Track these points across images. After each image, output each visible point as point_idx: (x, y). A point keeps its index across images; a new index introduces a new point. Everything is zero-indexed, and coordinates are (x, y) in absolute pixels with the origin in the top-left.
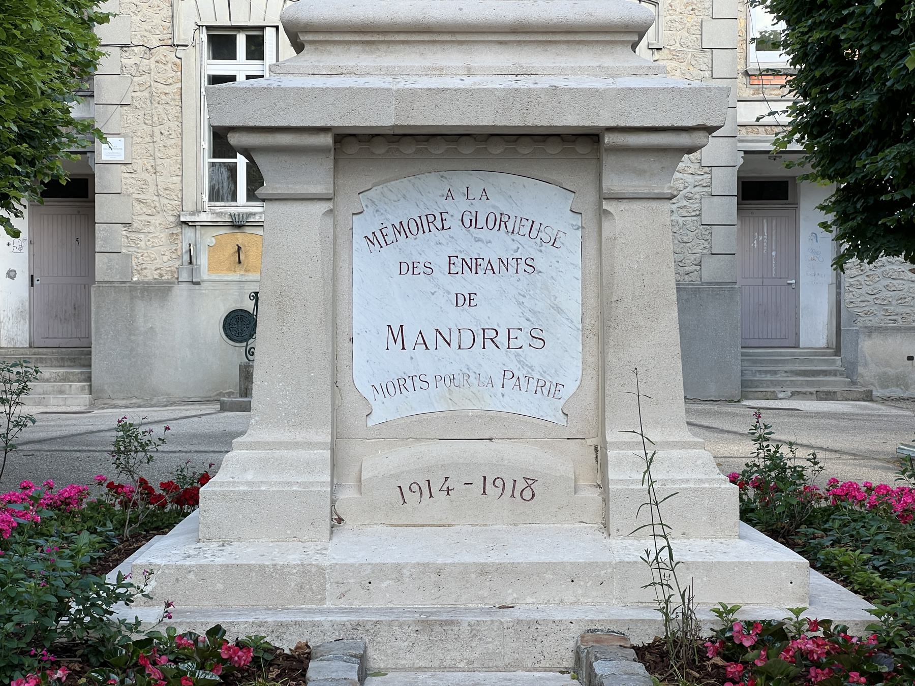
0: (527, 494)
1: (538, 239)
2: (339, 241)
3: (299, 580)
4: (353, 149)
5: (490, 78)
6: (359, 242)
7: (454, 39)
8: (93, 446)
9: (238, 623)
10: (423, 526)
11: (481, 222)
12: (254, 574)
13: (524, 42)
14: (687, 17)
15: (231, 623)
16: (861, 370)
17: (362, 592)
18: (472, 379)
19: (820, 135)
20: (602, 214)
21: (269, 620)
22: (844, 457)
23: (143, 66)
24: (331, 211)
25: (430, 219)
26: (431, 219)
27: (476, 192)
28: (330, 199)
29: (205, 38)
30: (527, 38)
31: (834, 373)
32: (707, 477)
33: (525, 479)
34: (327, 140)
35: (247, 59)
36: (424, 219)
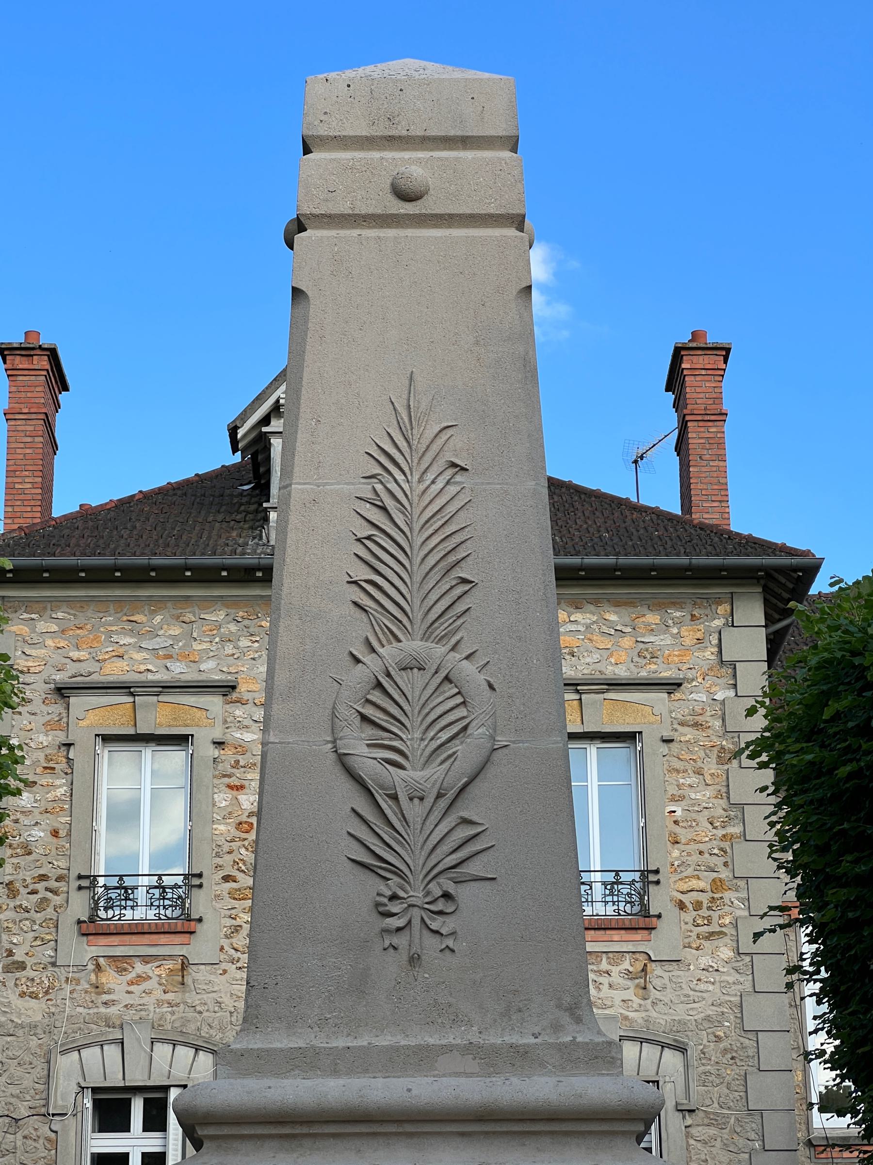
7: (401, 1130)
13: (494, 1133)
14: (726, 1069)
23: (6, 1144)
29: (89, 1104)
35: (144, 1131)
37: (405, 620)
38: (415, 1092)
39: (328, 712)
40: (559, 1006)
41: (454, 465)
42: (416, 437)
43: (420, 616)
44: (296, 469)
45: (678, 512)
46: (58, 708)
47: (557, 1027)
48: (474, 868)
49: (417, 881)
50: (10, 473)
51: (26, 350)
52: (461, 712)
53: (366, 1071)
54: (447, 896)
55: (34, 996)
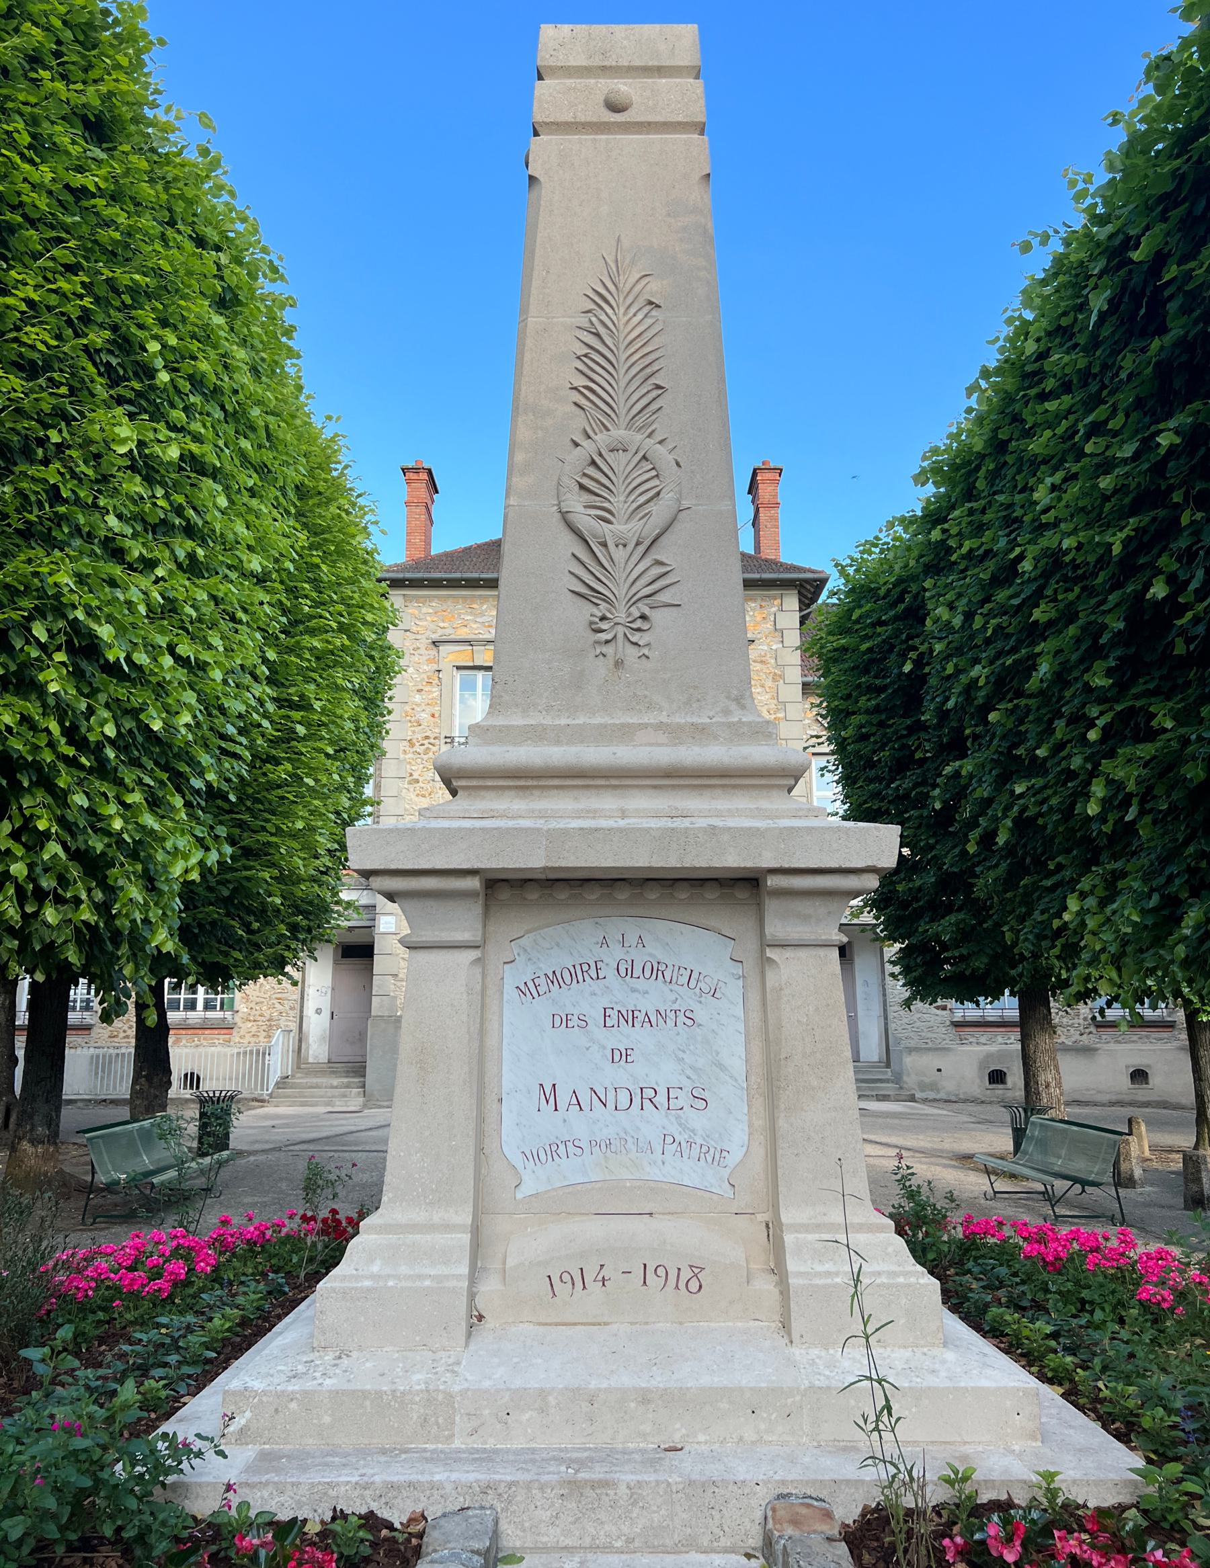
0: (694, 1286)
1: (697, 990)
2: (489, 992)
3: (422, 1411)
4: (504, 894)
5: (644, 820)
6: (510, 992)
8: (356, 1145)
9: (338, 1484)
10: (575, 1324)
11: (637, 972)
12: (368, 1403)
15: (328, 1483)
16: (905, 1078)
17: (499, 1426)
18: (630, 1145)
19: (886, 908)
20: (765, 962)
21: (377, 1479)
22: (917, 1155)
24: (479, 959)
25: (584, 968)
26: (585, 967)
27: (632, 939)
28: (478, 947)
30: (682, 782)
31: (887, 1081)
32: (901, 1268)
33: (691, 1266)
34: (474, 883)
36: (578, 968)
37: (613, 415)
38: (619, 754)
39: (555, 483)
40: (728, 698)
41: (651, 303)
42: (622, 281)
43: (624, 412)
44: (531, 307)
45: (753, 553)
46: (434, 652)
47: (726, 712)
48: (664, 597)
49: (621, 607)
50: (408, 534)
51: (416, 470)
52: (655, 482)
53: (582, 742)
54: (643, 617)
55: (423, 796)
